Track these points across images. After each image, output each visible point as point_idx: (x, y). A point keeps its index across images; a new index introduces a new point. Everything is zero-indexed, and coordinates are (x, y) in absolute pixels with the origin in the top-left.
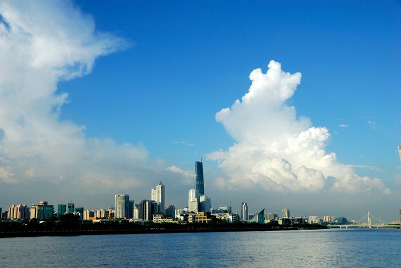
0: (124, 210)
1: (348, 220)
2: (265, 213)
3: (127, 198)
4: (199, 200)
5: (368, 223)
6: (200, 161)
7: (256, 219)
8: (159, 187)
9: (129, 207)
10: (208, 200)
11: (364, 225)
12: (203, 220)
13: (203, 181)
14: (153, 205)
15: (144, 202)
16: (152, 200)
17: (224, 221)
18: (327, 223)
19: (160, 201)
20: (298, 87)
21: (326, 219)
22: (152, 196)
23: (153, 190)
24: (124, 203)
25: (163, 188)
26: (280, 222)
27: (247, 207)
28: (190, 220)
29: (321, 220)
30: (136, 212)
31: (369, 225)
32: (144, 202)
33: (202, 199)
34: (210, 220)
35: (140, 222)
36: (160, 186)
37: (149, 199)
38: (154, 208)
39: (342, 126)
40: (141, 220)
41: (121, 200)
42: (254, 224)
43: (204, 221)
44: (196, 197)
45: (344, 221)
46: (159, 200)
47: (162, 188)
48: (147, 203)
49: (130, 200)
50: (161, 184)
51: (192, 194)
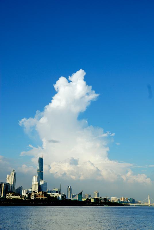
1: (136, 200)
4: (39, 183)
6: (42, 157)
7: (77, 198)
10: (45, 184)
11: (146, 204)
12: (41, 197)
16: (7, 182)
17: (56, 198)
18: (122, 202)
19: (13, 184)
21: (122, 199)
22: (7, 180)
23: (8, 175)
25: (15, 174)
26: (92, 201)
27: (71, 189)
28: (32, 197)
29: (119, 200)
31: (149, 204)
33: (42, 183)
34: (46, 197)
36: (13, 173)
37: (5, 182)
44: (38, 181)
46: (11, 183)
47: (14, 174)
48: (3, 184)
50: (14, 171)
51: (35, 179)
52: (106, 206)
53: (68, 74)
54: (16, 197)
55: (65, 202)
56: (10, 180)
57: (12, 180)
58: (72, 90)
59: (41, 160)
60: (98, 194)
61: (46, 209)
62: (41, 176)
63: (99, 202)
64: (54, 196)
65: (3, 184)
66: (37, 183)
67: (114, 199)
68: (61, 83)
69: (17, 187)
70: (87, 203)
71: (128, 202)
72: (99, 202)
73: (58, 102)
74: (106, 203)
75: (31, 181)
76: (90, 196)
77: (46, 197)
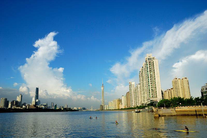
0: (4, 104)
1: (86, 108)
2: (57, 106)
3: (6, 99)
4: (36, 101)
5: (91, 109)
6: (38, 87)
7: (53, 108)
8: (20, 96)
9: (6, 103)
10: (39, 101)
11: (90, 110)
13: (38, 94)
14: (17, 102)
15: (13, 101)
16: (17, 100)
17: (41, 108)
18: (79, 110)
19: (20, 101)
20: (64, 70)
21: (79, 108)
22: (17, 99)
24: (5, 101)
25: (22, 96)
26: (62, 109)
27: (53, 104)
28: (27, 108)
29: (78, 109)
30: (10, 105)
31: (92, 110)
32: (13, 101)
33: (37, 101)
34: (202, 104)
35: (4, 108)
36: (21, 95)
37: (15, 100)
38: (17, 103)
39: (12, 78)
40: (5, 107)
41: (4, 100)
42: (52, 109)
43: (33, 108)
45: (84, 109)
46: (19, 101)
47: (21, 96)
48: (15, 101)
49: (7, 100)
50: (21, 94)
51: (34, 99)
52: (69, 112)
53: (42, 36)
54: (17, 108)
55: (47, 110)
56: (18, 99)
57: (20, 99)
58: (47, 46)
59: (37, 89)
60: (67, 106)
61: (17, 114)
62: (37, 97)
63: (66, 110)
64: (41, 107)
65: (15, 101)
66: (35, 101)
67: (75, 108)
68: (38, 43)
69: (22, 103)
70: (60, 110)
71: (82, 110)
72: (66, 110)
73: (40, 54)
74: (70, 110)
75: (32, 100)
76: (60, 107)
77: (202, 104)
